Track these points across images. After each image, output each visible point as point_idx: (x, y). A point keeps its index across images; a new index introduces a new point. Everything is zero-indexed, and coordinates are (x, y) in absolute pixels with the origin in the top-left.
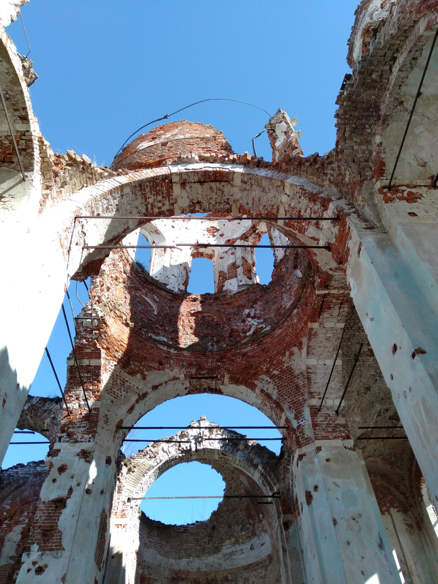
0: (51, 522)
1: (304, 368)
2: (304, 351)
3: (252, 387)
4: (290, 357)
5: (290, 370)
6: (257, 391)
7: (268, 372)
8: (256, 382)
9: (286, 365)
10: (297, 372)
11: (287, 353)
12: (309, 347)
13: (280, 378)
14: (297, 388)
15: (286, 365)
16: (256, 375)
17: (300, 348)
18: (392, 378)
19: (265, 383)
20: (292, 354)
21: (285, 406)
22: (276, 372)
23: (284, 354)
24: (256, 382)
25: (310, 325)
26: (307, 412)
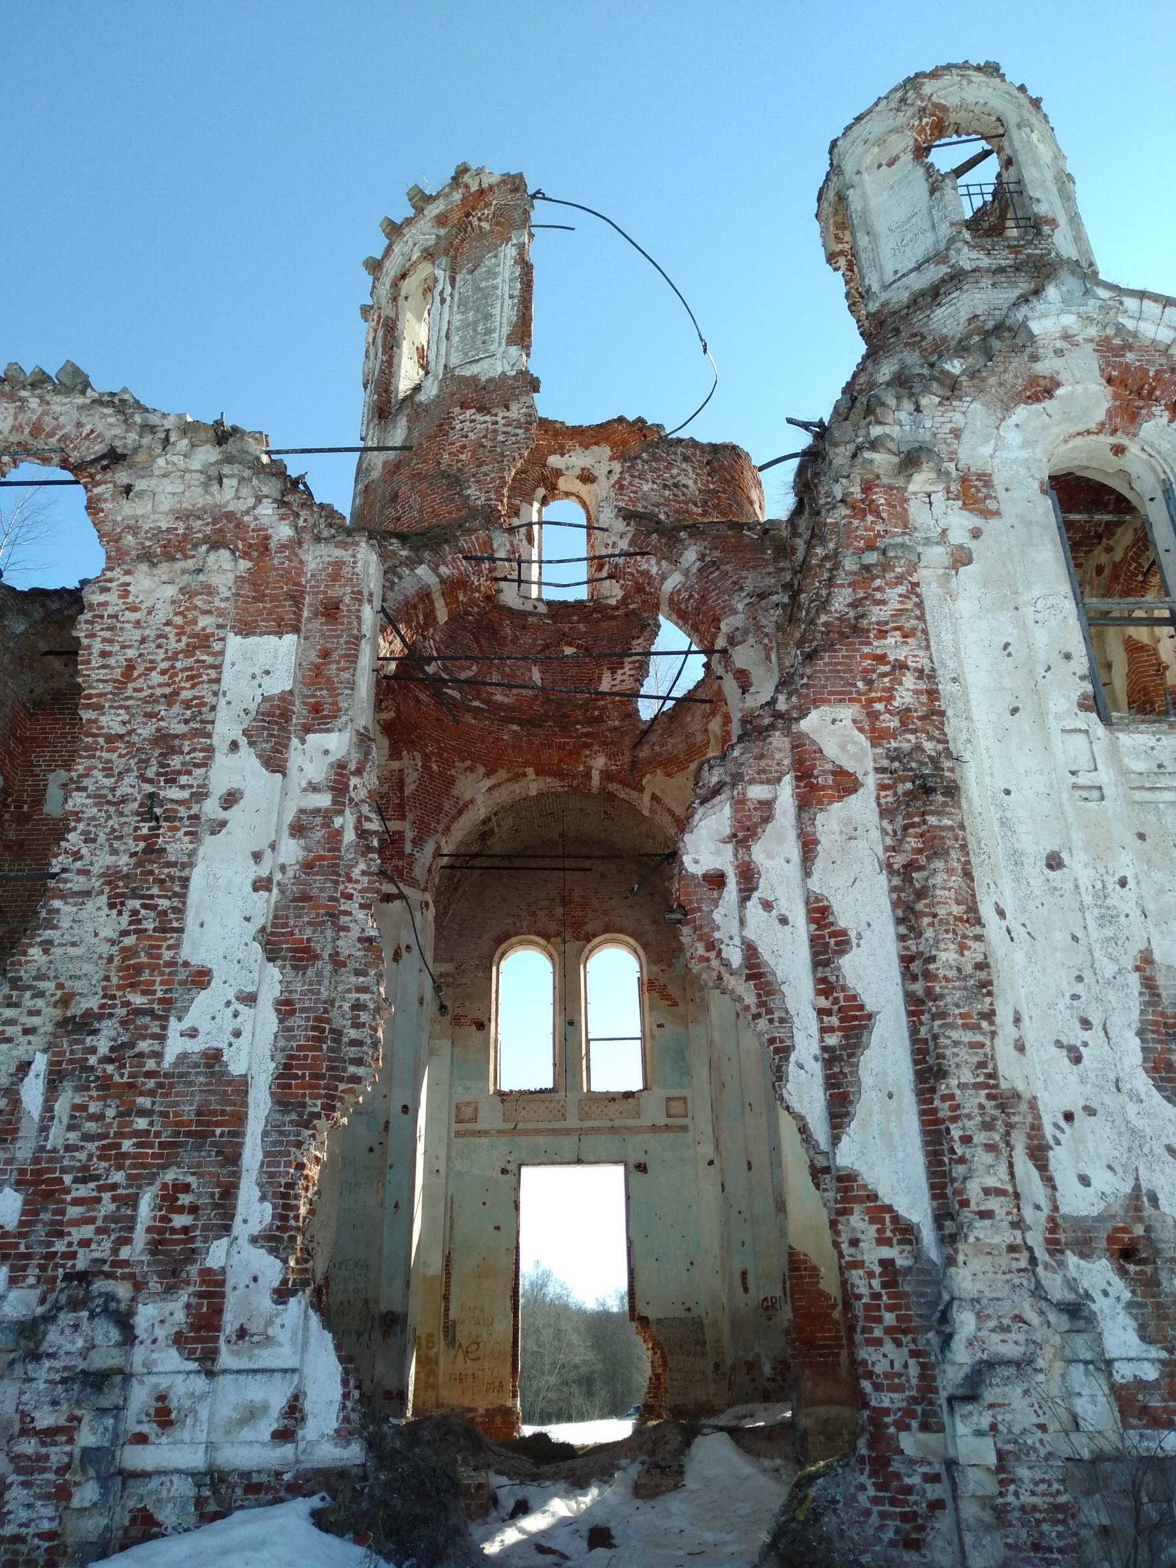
0: (849, 1022)
1: (467, 797)
2: (489, 783)
3: (395, 754)
4: (466, 770)
5: (451, 782)
6: (396, 765)
7: (427, 757)
8: (405, 753)
9: (453, 772)
10: (455, 793)
11: (468, 763)
12: (499, 785)
13: (431, 778)
14: (439, 808)
15: (453, 772)
16: (412, 745)
17: (488, 775)
18: (750, 1169)
19: (411, 766)
20: (472, 769)
21: (410, 816)
22: (435, 767)
23: (463, 760)
24: (405, 753)
25: (530, 771)
26: (429, 848)
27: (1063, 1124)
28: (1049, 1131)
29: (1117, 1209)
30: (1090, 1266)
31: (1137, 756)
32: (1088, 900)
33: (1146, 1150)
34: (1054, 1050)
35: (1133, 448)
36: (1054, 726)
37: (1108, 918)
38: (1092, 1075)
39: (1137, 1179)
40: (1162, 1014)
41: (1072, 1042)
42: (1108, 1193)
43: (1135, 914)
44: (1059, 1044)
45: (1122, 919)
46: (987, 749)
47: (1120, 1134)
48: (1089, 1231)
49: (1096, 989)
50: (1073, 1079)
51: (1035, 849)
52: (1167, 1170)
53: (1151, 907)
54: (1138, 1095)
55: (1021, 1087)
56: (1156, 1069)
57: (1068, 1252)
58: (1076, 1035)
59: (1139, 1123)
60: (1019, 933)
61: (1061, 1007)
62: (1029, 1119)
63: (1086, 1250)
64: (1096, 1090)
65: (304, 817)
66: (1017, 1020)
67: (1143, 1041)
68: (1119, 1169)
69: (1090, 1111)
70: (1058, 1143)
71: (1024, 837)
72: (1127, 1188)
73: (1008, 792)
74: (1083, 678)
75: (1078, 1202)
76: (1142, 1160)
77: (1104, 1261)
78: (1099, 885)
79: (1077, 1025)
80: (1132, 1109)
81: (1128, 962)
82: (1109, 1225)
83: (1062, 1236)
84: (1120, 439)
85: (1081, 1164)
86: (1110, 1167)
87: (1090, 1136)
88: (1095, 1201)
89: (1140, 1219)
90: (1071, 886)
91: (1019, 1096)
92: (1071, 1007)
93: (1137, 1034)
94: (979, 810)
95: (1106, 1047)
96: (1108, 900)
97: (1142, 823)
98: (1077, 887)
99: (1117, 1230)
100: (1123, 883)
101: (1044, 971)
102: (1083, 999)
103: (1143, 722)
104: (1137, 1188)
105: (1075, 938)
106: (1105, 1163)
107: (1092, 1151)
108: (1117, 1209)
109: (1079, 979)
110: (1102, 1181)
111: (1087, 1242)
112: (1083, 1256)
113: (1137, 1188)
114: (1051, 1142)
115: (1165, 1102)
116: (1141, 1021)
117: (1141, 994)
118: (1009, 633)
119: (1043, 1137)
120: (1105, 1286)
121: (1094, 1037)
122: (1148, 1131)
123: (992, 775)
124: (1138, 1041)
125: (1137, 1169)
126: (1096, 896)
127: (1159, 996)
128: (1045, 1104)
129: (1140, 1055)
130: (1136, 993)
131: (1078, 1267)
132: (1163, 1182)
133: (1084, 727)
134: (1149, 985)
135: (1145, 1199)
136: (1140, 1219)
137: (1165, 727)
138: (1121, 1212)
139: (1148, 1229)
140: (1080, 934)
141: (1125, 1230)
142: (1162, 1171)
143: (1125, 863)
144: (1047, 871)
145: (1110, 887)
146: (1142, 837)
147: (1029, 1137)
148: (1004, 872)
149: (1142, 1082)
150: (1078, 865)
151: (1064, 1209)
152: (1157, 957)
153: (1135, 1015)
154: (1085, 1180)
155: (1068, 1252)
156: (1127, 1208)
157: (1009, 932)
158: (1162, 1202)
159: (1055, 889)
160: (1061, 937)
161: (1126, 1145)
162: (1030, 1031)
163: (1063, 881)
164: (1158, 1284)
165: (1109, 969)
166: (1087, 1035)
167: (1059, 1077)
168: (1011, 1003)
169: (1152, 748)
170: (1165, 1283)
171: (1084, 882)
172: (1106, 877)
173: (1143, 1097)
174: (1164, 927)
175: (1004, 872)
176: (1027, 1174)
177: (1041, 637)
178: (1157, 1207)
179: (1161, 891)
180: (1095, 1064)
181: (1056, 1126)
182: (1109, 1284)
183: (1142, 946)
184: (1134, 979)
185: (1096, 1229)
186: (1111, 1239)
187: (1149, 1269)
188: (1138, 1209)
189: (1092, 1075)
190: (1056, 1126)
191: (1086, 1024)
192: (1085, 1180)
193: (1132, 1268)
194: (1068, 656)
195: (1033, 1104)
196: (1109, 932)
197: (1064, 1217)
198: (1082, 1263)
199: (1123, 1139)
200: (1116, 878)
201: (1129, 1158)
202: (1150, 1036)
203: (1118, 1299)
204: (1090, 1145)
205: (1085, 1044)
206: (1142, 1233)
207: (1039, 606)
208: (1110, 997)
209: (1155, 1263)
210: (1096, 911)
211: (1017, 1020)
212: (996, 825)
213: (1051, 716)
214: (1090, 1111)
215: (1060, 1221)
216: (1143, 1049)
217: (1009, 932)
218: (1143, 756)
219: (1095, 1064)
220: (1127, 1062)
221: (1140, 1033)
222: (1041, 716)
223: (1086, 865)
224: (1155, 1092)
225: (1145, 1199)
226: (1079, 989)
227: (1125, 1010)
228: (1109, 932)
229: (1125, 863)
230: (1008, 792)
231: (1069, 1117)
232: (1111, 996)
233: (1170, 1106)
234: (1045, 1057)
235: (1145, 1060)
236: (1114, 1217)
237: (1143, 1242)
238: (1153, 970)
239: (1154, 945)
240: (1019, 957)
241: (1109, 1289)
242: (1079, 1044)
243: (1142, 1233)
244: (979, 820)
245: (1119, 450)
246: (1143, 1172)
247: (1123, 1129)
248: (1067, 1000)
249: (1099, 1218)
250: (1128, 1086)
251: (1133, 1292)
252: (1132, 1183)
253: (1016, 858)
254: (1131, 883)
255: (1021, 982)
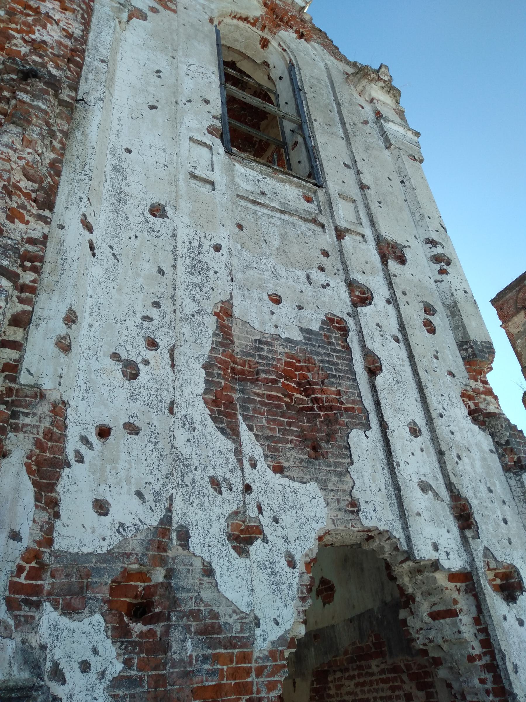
27: (94, 439)
28: (72, 444)
29: (135, 545)
30: (74, 625)
31: (247, 181)
32: (182, 250)
33: (188, 480)
34: (108, 362)
35: (274, 43)
36: (185, 135)
37: (198, 268)
38: (145, 393)
39: (169, 510)
40: (231, 356)
41: (132, 357)
42: (128, 524)
43: (223, 274)
44: (115, 356)
45: (211, 273)
46: (119, 119)
47: (161, 458)
48: (88, 575)
49: (170, 317)
50: (122, 394)
51: (142, 191)
52: (207, 504)
53: (238, 275)
54: (192, 423)
55: (47, 384)
56: (215, 402)
57: (47, 606)
58: (137, 352)
59: (186, 450)
60: (101, 247)
61: (130, 324)
62: (47, 423)
63: (76, 602)
64: (146, 408)
65: (44, 408)
66: (71, 318)
67: (208, 374)
68: (149, 497)
69: (132, 429)
70: (80, 459)
71: (133, 185)
72: (153, 520)
73: (129, 151)
74: (215, 117)
75: (81, 533)
76: (182, 490)
77: (98, 618)
78: (196, 243)
79: (142, 343)
80: (181, 436)
81: (209, 306)
82: (118, 567)
83: (46, 583)
84: (266, 34)
85: (104, 487)
86: (139, 494)
87: (124, 456)
88: (108, 534)
89: (163, 561)
90: (170, 233)
91: (42, 396)
92: (141, 326)
93: (204, 367)
94: (93, 144)
95: (169, 369)
96: (201, 256)
97: (242, 218)
98: (174, 235)
99: (128, 575)
100: (218, 248)
101: (120, 290)
102: (155, 322)
103: (255, 161)
104: (167, 520)
105: (161, 271)
106: (133, 489)
107: (122, 474)
108: (135, 545)
109: (156, 305)
110: (127, 510)
111: (82, 590)
112: (69, 611)
113: (167, 520)
114: (71, 457)
115: (218, 433)
116: (210, 357)
117: (215, 335)
118: (163, 64)
119: (62, 450)
120: (87, 655)
121: (159, 358)
122: (195, 460)
123: (117, 136)
124: (203, 372)
125: (171, 499)
126: (191, 249)
127: (232, 341)
128: (78, 414)
129: (202, 386)
130: (211, 333)
131: (55, 627)
132: (199, 517)
133: (209, 143)
134: (224, 333)
135: (174, 536)
136: (163, 561)
137: (270, 170)
138: (139, 550)
139: (169, 575)
140: (167, 269)
141: (142, 576)
142: (201, 505)
143: (223, 235)
144: (148, 215)
145: (205, 248)
146: (240, 227)
147: (38, 444)
148: (105, 202)
149: (200, 412)
150: (180, 221)
151: (61, 543)
152: (236, 311)
153: (206, 350)
154: (101, 507)
155: (47, 606)
156: (148, 545)
157: (92, 248)
158: (194, 541)
159: (153, 230)
160: (147, 267)
161: (165, 470)
162: (83, 336)
163: (162, 226)
164: (166, 648)
165: (190, 308)
166: (150, 355)
167: (105, 390)
168: (68, 301)
169: (259, 181)
170: (175, 647)
171: (184, 234)
172: (203, 240)
173: (197, 426)
174: (246, 293)
175: (105, 202)
176: (17, 490)
177: (188, 84)
178: (186, 546)
179: (248, 267)
180: (152, 383)
181: (85, 440)
182: (95, 651)
183: (225, 297)
184: (211, 322)
185: (99, 572)
186: (116, 589)
187: (158, 628)
188: (162, 547)
189: (145, 393)
190: (85, 440)
191: (152, 344)
192: (101, 507)
193: (137, 628)
194: (207, 102)
195: (59, 409)
196: (196, 279)
197: (57, 555)
198: (64, 621)
199: (164, 463)
200: (213, 243)
201: (165, 485)
202: (216, 371)
203: (102, 674)
204: (122, 466)
205: (146, 362)
206: (161, 579)
207: (191, 68)
208: (185, 330)
209: (169, 619)
210: (188, 261)
211: (71, 318)
212: (109, 169)
213: (183, 127)
214: (132, 429)
215: (47, 558)
216: (207, 382)
217: (92, 248)
218: (251, 182)
219: (152, 383)
220: (187, 391)
221: (206, 367)
222: (175, 121)
223: (188, 226)
224: (210, 422)
225: (174, 536)
226: (154, 313)
227: (197, 346)
228: (196, 279)
229: (223, 235)
230: (129, 151)
231: (104, 433)
232: (186, 329)
233: (223, 437)
234: (94, 365)
235: (207, 391)
236: (128, 555)
237: (161, 591)
238: (231, 322)
239: (235, 302)
240: (96, 271)
241: (93, 660)
242: (139, 360)
243: (161, 579)
244: (90, 151)
245: (265, 43)
246: (178, 505)
247: (166, 452)
248: (138, 320)
249: (108, 557)
250: (184, 412)
251: (127, 663)
252: (160, 514)
253: (121, 198)
254: (224, 250)
255: (90, 292)
